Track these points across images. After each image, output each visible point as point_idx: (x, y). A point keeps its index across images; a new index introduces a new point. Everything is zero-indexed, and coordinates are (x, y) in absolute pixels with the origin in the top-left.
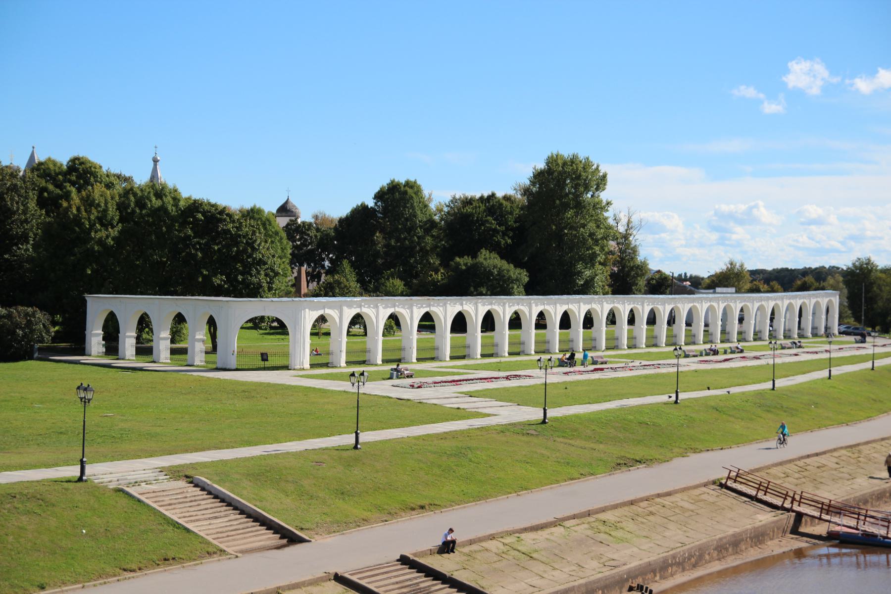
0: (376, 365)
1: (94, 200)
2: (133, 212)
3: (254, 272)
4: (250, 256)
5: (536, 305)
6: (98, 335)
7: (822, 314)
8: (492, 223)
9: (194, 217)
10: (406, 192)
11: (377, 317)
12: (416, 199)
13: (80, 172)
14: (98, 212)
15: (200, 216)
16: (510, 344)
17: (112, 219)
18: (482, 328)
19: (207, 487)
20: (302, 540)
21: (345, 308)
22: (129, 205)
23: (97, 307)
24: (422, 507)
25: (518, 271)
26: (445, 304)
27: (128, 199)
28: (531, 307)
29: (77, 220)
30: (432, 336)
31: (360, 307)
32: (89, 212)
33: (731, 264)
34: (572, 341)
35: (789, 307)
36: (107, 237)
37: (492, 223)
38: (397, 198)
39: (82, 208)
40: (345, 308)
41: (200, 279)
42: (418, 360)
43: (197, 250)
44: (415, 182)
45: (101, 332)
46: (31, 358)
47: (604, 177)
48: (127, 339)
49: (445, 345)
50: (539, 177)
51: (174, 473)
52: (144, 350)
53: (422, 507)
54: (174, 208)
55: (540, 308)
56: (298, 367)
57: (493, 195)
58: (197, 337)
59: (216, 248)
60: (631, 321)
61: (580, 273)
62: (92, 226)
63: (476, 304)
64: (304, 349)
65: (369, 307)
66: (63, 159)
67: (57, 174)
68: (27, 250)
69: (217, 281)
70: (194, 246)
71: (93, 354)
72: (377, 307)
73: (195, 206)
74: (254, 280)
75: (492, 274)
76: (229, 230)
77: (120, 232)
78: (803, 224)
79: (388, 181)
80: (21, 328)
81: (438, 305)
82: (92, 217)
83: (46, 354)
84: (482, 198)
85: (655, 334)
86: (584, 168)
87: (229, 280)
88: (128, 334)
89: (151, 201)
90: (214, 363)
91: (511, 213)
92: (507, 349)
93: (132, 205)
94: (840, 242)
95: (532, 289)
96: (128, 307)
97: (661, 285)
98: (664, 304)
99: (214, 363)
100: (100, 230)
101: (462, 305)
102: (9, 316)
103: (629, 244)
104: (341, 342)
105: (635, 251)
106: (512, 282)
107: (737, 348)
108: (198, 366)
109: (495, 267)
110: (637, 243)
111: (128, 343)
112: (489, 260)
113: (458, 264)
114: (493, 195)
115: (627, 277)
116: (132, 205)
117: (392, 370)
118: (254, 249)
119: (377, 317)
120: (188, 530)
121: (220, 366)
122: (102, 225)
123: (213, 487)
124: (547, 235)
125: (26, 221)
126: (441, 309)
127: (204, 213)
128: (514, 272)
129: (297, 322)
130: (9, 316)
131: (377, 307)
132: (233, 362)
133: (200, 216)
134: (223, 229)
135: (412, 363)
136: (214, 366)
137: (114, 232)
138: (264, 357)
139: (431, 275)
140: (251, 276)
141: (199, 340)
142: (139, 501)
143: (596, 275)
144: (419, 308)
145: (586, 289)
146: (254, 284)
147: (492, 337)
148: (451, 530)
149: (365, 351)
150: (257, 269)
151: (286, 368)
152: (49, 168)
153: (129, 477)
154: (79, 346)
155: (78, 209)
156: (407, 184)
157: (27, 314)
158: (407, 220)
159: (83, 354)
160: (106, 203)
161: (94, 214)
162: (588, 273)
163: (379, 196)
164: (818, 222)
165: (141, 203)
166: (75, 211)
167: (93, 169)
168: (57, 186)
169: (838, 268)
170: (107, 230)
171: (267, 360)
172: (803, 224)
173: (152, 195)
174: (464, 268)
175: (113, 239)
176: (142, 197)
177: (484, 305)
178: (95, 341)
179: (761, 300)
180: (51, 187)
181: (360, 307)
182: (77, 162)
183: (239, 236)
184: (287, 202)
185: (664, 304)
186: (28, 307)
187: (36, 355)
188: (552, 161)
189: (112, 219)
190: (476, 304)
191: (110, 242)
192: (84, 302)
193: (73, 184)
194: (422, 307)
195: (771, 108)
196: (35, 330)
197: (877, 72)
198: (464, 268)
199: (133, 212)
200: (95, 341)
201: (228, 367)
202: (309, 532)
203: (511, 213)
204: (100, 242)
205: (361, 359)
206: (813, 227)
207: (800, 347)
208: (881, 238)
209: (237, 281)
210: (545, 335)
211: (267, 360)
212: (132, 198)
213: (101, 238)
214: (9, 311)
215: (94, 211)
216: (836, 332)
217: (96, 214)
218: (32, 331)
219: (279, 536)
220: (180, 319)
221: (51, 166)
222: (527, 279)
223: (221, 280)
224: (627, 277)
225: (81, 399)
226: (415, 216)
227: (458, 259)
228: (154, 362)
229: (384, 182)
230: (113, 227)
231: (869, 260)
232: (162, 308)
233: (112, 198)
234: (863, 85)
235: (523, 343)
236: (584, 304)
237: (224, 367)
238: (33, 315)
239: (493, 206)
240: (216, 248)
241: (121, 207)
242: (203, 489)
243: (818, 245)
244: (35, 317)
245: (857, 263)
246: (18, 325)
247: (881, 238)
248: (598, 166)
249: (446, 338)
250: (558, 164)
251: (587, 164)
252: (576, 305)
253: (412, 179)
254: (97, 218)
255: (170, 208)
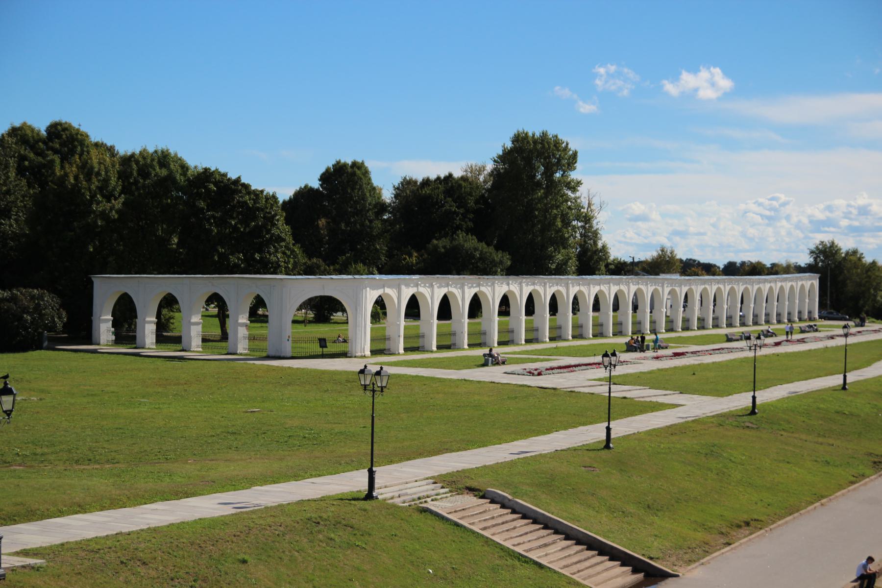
0: (432, 352)
1: (92, 168)
2: (136, 182)
3: (272, 250)
4: (268, 231)
5: (550, 287)
6: (107, 321)
7: (679, 307)
8: (451, 206)
9: (206, 188)
10: (354, 174)
11: (432, 298)
12: (364, 181)
13: (64, 139)
14: (99, 181)
15: (212, 186)
16: (373, 340)
17: (114, 189)
18: (550, 311)
19: (506, 502)
20: (664, 575)
21: (403, 287)
22: (131, 173)
23: (106, 290)
24: (747, 524)
25: (500, 254)
26: (493, 284)
27: (131, 166)
28: (519, 288)
29: (76, 190)
30: (416, 323)
31: (417, 285)
32: (89, 180)
33: (662, 251)
34: (454, 334)
35: (732, 292)
36: (111, 209)
37: (451, 206)
38: (345, 179)
39: (81, 177)
40: (403, 287)
41: (216, 258)
42: (406, 349)
43: (211, 224)
44: (363, 163)
45: (110, 317)
46: (39, 347)
47: (575, 154)
48: (147, 326)
49: (494, 330)
50: (506, 157)
51: (456, 483)
52: (166, 334)
53: (747, 524)
54: (182, 177)
55: (554, 289)
56: (359, 354)
57: (450, 175)
58: (240, 321)
59: (233, 223)
60: (530, 309)
61: (551, 257)
62: (93, 196)
63: (521, 283)
64: (365, 333)
65: (425, 286)
66: (41, 125)
67: (37, 142)
68: (11, 226)
69: (233, 259)
70: (208, 220)
71: (102, 342)
72: (432, 286)
73: (206, 175)
74: (274, 259)
75: (473, 257)
76: (245, 202)
77: (123, 204)
78: (630, 220)
79: (334, 162)
80: (28, 313)
81: (487, 285)
82: (93, 187)
83: (53, 344)
84: (438, 178)
85: (558, 323)
86: (555, 146)
87: (245, 260)
88: (148, 319)
89: (155, 170)
90: (262, 350)
91: (470, 194)
92: (466, 341)
93: (135, 174)
94: (667, 238)
95: (514, 270)
96: (147, 290)
97: (621, 269)
98: (680, 286)
99: (262, 350)
100: (102, 202)
101: (508, 284)
102: (13, 299)
103: (591, 227)
104: (399, 325)
105: (596, 234)
106: (495, 266)
107: (768, 331)
108: (241, 354)
109: (476, 249)
110: (599, 226)
111: (148, 330)
112: (470, 243)
113: (436, 247)
114: (450, 175)
115: (592, 261)
116: (135, 174)
117: (484, 355)
118: (274, 225)
119: (432, 298)
120: (540, 566)
121: (272, 354)
122: (103, 196)
123: (517, 503)
124: (514, 214)
125: (8, 192)
126: (489, 288)
127: (216, 184)
128: (498, 256)
129: (358, 304)
130: (13, 299)
131: (432, 286)
132: (288, 350)
133: (212, 186)
134: (239, 202)
135: (464, 349)
136: (264, 354)
137: (118, 204)
138: (323, 342)
139: (405, 259)
140: (270, 255)
141: (242, 325)
142: (457, 525)
143: (570, 259)
144: (470, 288)
145: (560, 270)
146: (272, 263)
147: (479, 324)
148: (870, 560)
149: (385, 339)
150: (274, 247)
151: (344, 355)
152: (26, 135)
153: (409, 491)
154: (81, 331)
155: (76, 178)
156: (354, 164)
157: (33, 298)
158: (356, 202)
159: (91, 344)
160: (107, 172)
161: (95, 184)
162: (560, 257)
163: (326, 178)
164: (644, 218)
165: (144, 172)
166: (72, 181)
167: (79, 137)
168: (37, 154)
169: (695, 261)
170: (109, 201)
171: (326, 347)
172: (630, 220)
173: (155, 163)
174: (443, 250)
175: (117, 212)
176: (145, 165)
177: (527, 285)
178: (105, 329)
179: (759, 282)
180: (32, 155)
181: (417, 285)
182: (59, 127)
183: (258, 209)
184: (239, 178)
185: (680, 286)
186: (33, 288)
187: (46, 344)
188: (520, 140)
189: (114, 189)
190: (521, 283)
191: (114, 215)
192: (91, 283)
193: (56, 152)
194: (472, 286)
195: (586, 108)
196: (45, 315)
197: (680, 74)
198: (443, 250)
199: (136, 182)
200: (105, 329)
201: (282, 355)
202: (660, 561)
203: (470, 194)
204: (103, 215)
205: (478, 342)
206: (640, 223)
207: (816, 330)
208: (704, 234)
209: (255, 259)
210: (507, 324)
211: (326, 347)
212: (134, 166)
213: (104, 211)
214: (12, 294)
215: (94, 180)
216: (817, 316)
217: (97, 183)
218: (42, 316)
219: (630, 568)
220: (169, 302)
221: (29, 132)
222: (509, 263)
223: (239, 259)
224: (592, 261)
225: (365, 387)
226: (363, 199)
227: (435, 242)
228: (183, 350)
229: (330, 163)
230: (116, 199)
231: (833, 243)
232: (192, 289)
233: (113, 166)
234: (670, 88)
235: (512, 331)
236: (614, 284)
237: (277, 354)
238: (41, 297)
239: (452, 187)
240: (233, 223)
241: (123, 175)
242: (503, 506)
243: (646, 241)
244: (43, 300)
245: (820, 247)
246: (25, 310)
247: (704, 234)
248: (567, 144)
249: (494, 322)
250: (528, 142)
251: (557, 143)
252: (607, 286)
253: (359, 160)
254: (97, 187)
255: (178, 177)
